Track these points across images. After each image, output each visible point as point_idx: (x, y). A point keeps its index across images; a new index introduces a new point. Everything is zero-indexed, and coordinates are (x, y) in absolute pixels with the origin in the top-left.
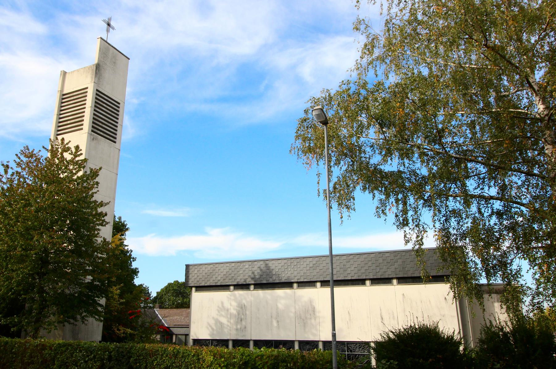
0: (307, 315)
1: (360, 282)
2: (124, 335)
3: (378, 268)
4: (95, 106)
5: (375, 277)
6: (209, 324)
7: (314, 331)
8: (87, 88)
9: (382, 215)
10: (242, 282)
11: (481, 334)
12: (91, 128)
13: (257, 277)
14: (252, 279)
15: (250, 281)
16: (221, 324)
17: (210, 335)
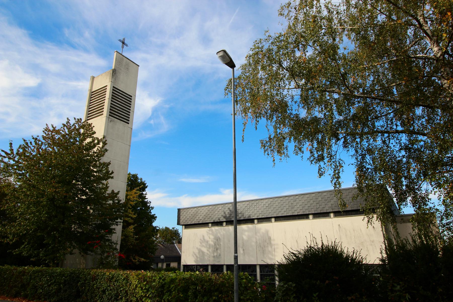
0: (266, 243)
1: (305, 217)
2: (139, 263)
3: (318, 205)
5: (316, 212)
6: (194, 253)
7: (270, 256)
8: (107, 86)
9: (299, 152)
10: (217, 220)
11: (381, 253)
12: (109, 113)
13: (228, 216)
14: (224, 217)
15: (222, 219)
16: (203, 252)
17: (195, 262)
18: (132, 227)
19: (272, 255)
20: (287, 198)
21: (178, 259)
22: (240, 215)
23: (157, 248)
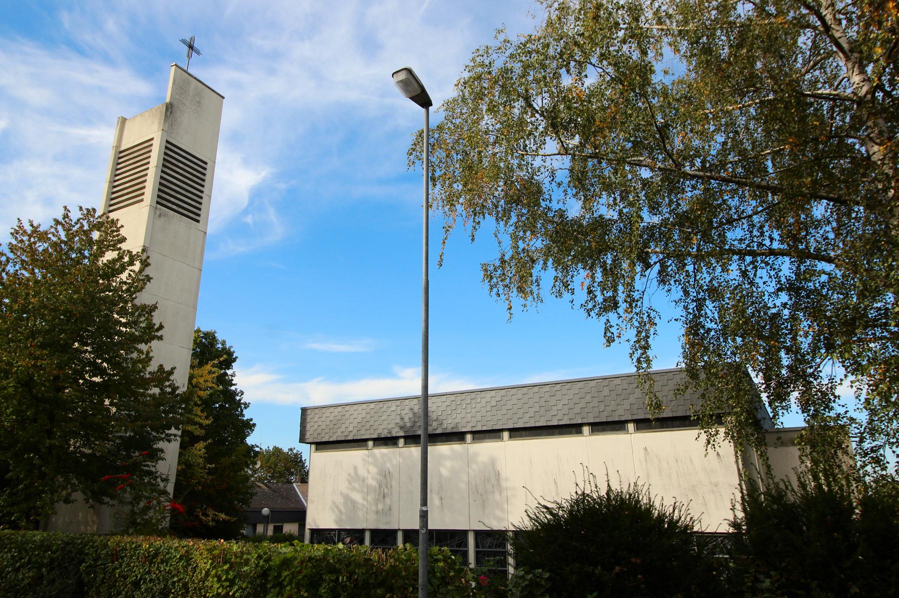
0: (490, 483)
1: (574, 430)
4: (164, 165)
5: (597, 420)
6: (334, 502)
7: (498, 513)
8: (152, 139)
10: (385, 434)
11: (733, 509)
12: (156, 199)
13: (408, 425)
14: (401, 428)
16: (354, 503)
17: (337, 522)
18: (201, 445)
19: (502, 510)
20: (536, 389)
21: (300, 515)
22: (435, 424)
23: (255, 491)
